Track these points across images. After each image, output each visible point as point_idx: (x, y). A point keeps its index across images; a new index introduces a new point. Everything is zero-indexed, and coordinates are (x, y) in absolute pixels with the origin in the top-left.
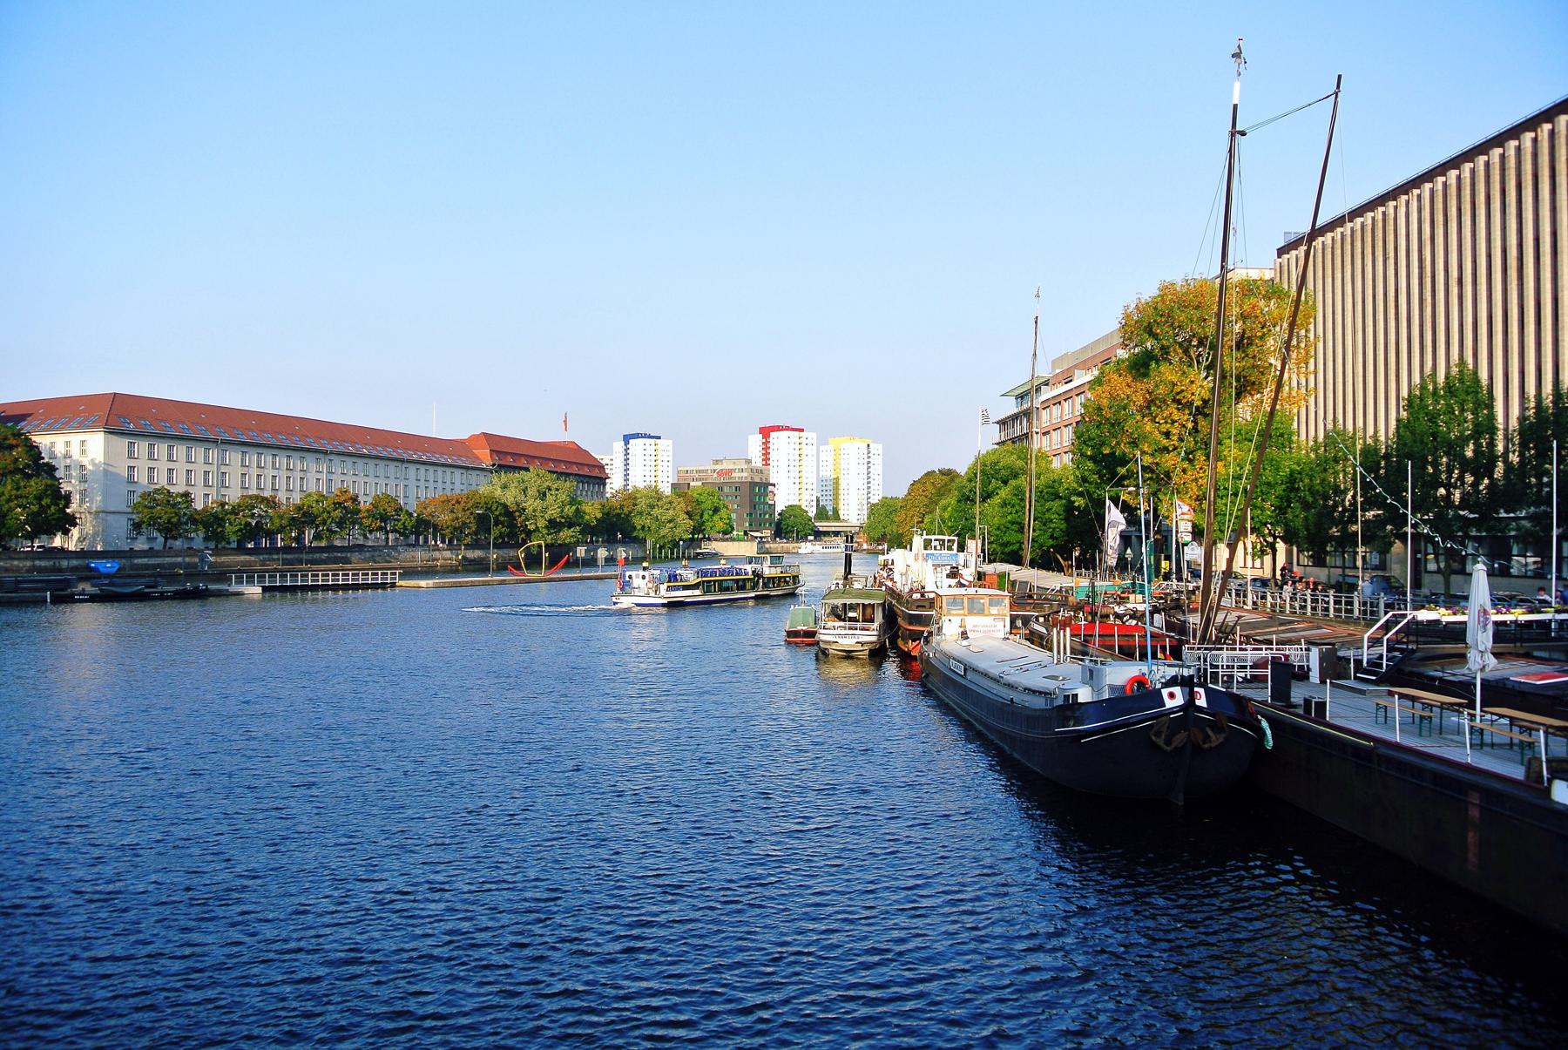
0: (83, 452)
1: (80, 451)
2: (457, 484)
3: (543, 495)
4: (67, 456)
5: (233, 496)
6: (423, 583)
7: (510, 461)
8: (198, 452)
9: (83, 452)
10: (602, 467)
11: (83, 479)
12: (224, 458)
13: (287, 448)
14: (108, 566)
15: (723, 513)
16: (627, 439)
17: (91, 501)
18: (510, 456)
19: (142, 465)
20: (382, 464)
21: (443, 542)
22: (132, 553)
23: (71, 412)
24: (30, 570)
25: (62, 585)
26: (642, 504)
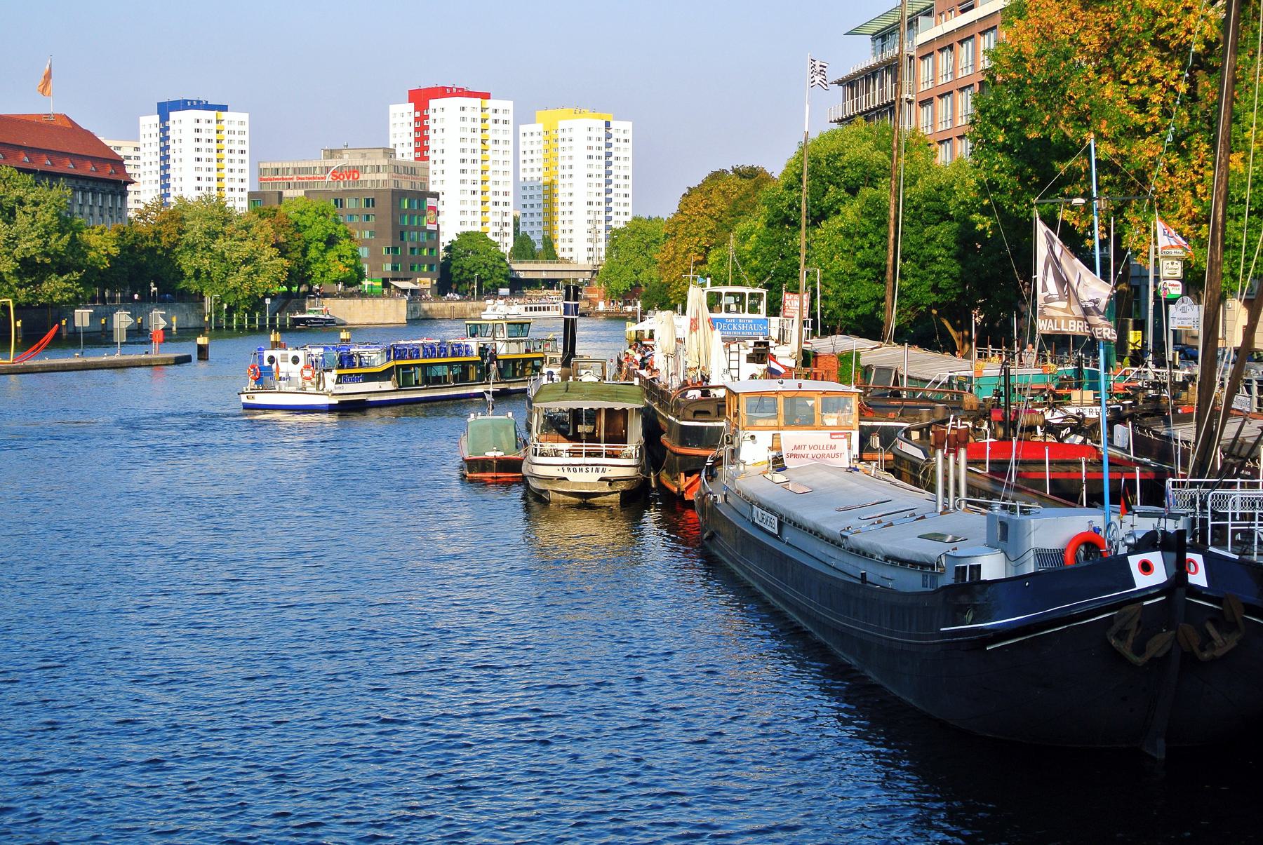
10: (118, 163)
15: (344, 247)
16: (164, 110)
26: (195, 231)
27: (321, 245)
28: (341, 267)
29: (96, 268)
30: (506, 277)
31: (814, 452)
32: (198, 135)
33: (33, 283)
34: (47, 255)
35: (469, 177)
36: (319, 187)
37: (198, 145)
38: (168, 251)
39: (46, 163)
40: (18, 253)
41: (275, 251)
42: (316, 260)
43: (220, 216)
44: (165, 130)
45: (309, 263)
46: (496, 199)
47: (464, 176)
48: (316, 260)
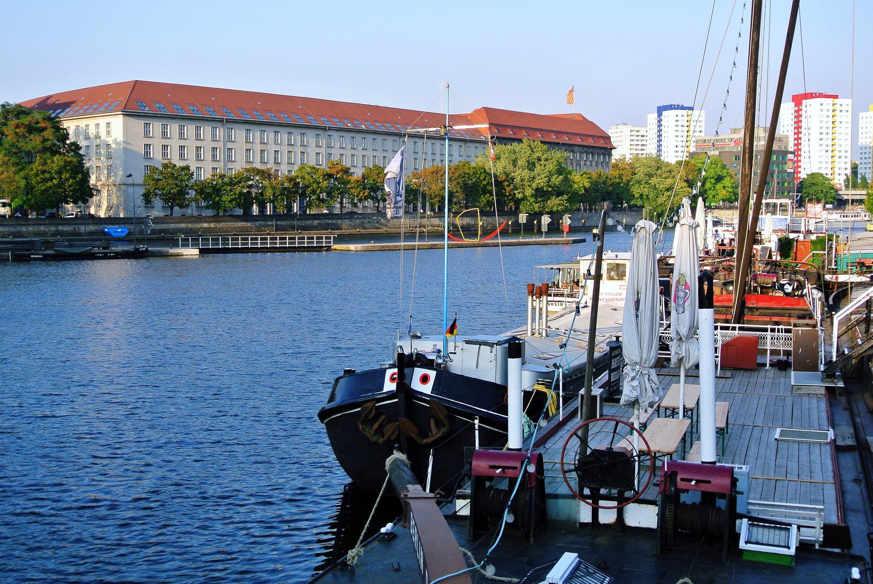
0: (108, 133)
1: (104, 133)
2: (449, 156)
3: (531, 166)
4: (98, 137)
5: (238, 166)
6: (352, 247)
7: (510, 133)
8: (206, 130)
9: (108, 133)
10: (607, 138)
11: (109, 157)
12: (230, 137)
13: (288, 126)
14: (119, 231)
15: (727, 182)
16: (660, 110)
17: (116, 176)
18: (506, 128)
19: (157, 143)
20: (379, 138)
21: (432, 210)
22: (141, 221)
23: (94, 100)
24: (54, 234)
25: (92, 244)
26: (640, 175)
27: (713, 181)
28: (724, 192)
29: (577, 193)
30: (834, 198)
31: (608, 297)
32: (677, 123)
33: (543, 201)
34: (550, 186)
35: (824, 142)
36: (727, 150)
38: (628, 184)
39: (553, 138)
40: (534, 186)
41: (685, 184)
42: (710, 189)
43: (658, 165)
44: (660, 121)
45: (706, 191)
46: (840, 154)
47: (821, 142)
48: (710, 189)
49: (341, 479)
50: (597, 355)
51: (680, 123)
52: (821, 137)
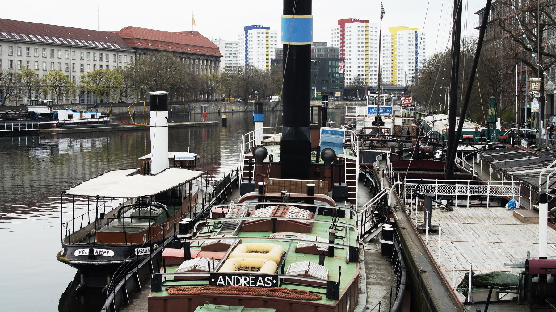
32: (259, 39)
37: (259, 42)
49: (64, 249)
50: (83, 226)
51: (261, 39)
52: (358, 37)
